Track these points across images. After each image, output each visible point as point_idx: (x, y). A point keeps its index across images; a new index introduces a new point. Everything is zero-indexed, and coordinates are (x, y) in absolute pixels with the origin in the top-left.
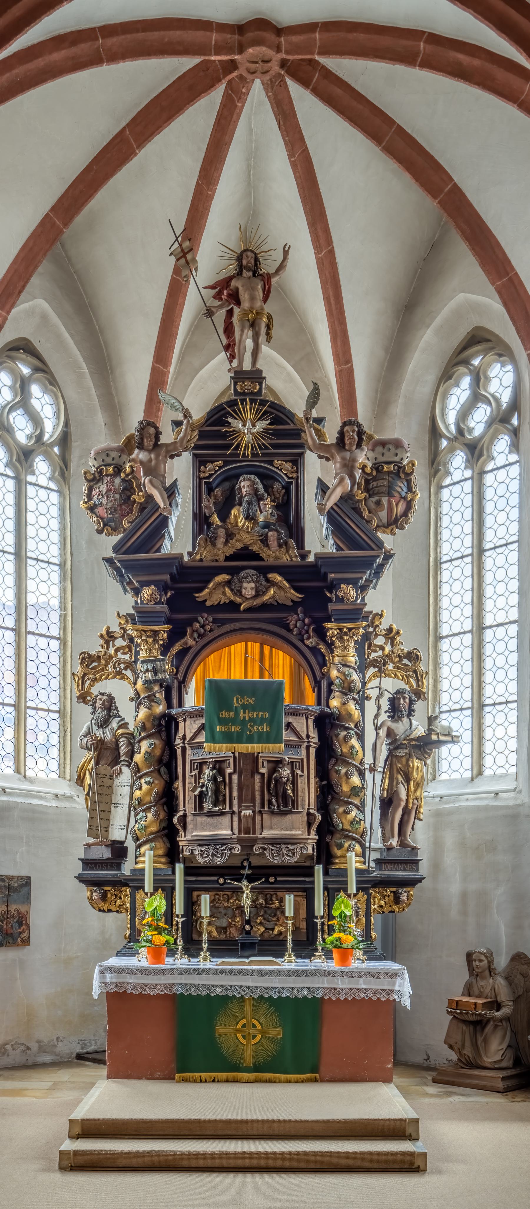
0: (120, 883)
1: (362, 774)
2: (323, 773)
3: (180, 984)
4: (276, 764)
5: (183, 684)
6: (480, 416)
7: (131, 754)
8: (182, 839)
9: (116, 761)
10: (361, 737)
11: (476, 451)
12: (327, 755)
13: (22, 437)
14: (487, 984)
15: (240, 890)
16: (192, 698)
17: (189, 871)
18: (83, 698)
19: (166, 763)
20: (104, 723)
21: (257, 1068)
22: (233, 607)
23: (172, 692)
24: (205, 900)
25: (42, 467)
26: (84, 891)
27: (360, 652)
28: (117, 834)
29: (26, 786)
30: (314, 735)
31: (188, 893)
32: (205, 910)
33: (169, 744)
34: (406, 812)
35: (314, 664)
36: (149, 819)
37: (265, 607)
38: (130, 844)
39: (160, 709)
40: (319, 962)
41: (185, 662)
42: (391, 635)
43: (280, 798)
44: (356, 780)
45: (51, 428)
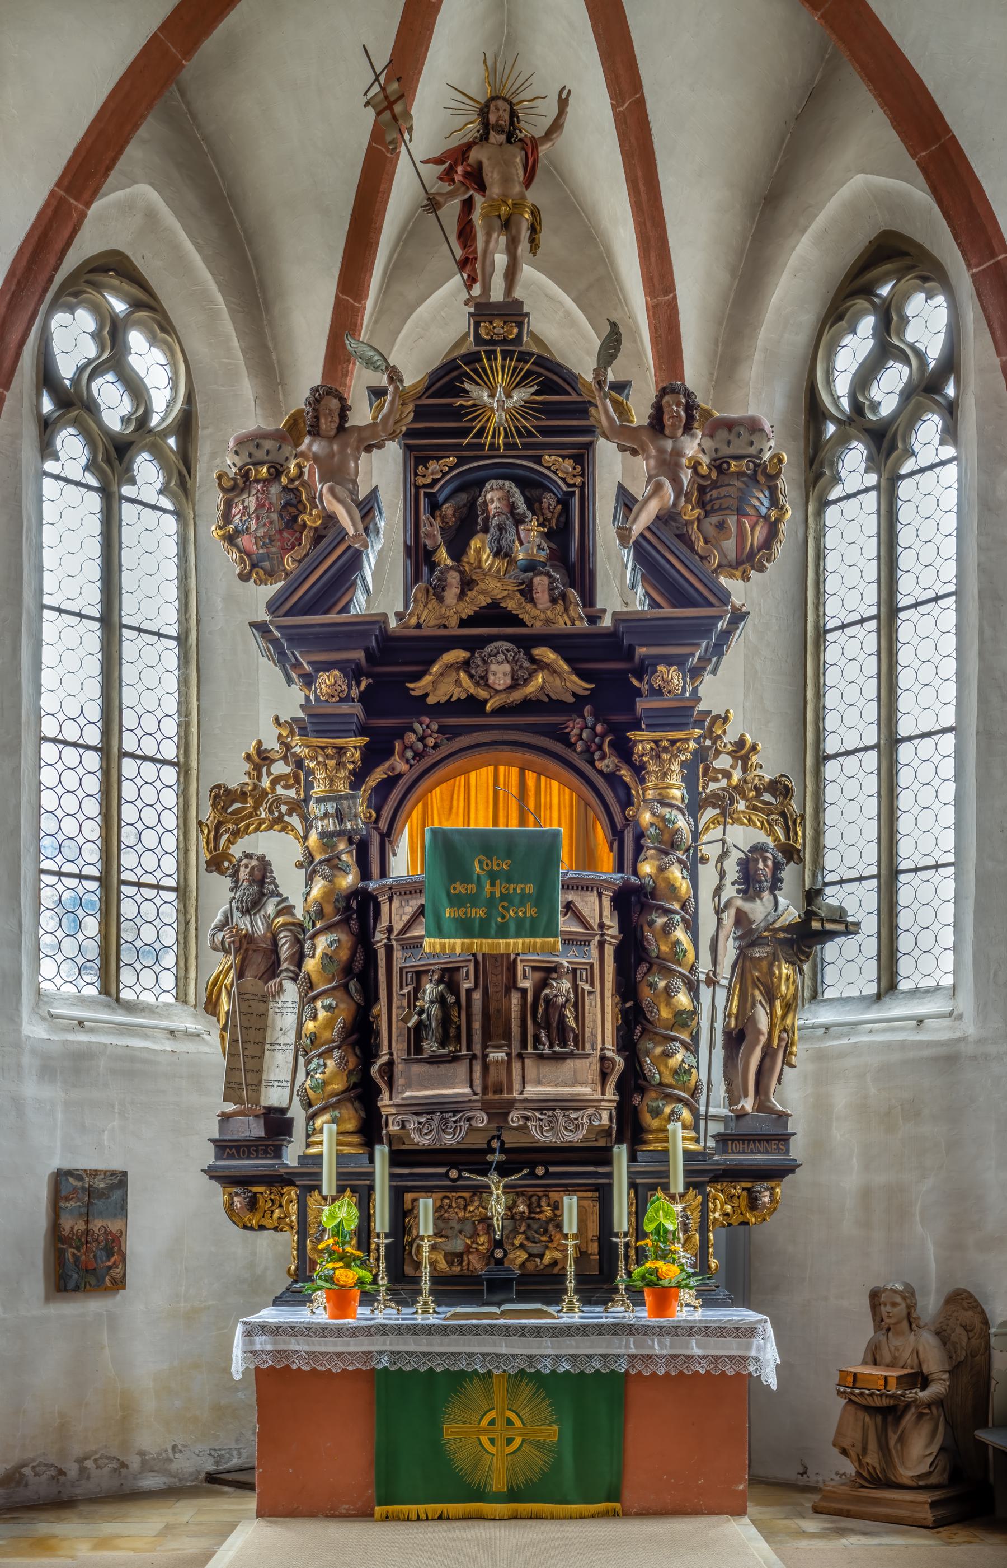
1: (693, 988)
2: (627, 989)
4: (548, 972)
5: (387, 837)
6: (887, 392)
7: (299, 959)
8: (386, 1103)
9: (273, 970)
10: (692, 927)
11: (887, 443)
12: (633, 956)
16: (403, 862)
17: (397, 1158)
19: (360, 974)
20: (252, 907)
21: (513, 1495)
22: (472, 705)
23: (369, 852)
25: (147, 473)
26: (217, 1194)
27: (690, 781)
28: (275, 1096)
30: (611, 922)
31: (397, 1195)
32: (425, 1224)
33: (363, 939)
34: (768, 1053)
36: (331, 1071)
37: (527, 706)
38: (298, 1113)
39: (348, 881)
40: (620, 1311)
41: (391, 800)
42: (742, 752)
44: (683, 999)
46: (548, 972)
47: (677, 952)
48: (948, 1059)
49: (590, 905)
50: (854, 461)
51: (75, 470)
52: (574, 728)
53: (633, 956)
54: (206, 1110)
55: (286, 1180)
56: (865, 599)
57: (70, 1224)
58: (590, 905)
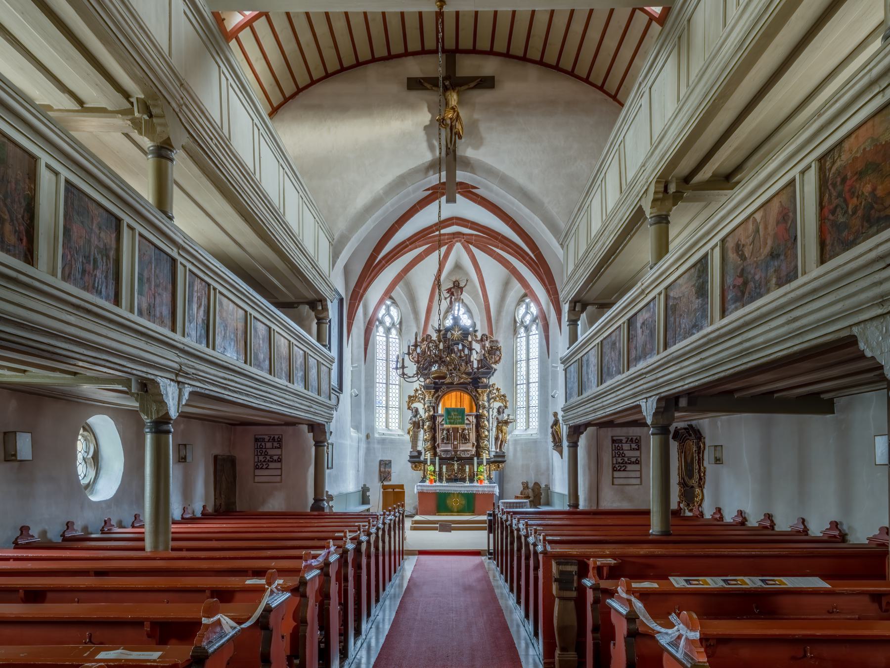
0: (421, 462)
1: (489, 431)
2: (477, 431)
3: (438, 490)
4: (464, 430)
5: (438, 405)
6: (528, 318)
7: (423, 425)
8: (438, 450)
9: (419, 427)
10: (488, 421)
11: (527, 329)
12: (478, 426)
13: (388, 324)
14: (526, 491)
15: (219, 623)
16: (440, 410)
17: (441, 459)
18: (409, 408)
19: (433, 429)
20: (415, 416)
21: (458, 512)
22: (452, 383)
23: (435, 408)
24: (444, 467)
25: (394, 332)
26: (410, 464)
27: (488, 396)
28: (420, 448)
29: (292, 340)
30: (475, 421)
31: (440, 465)
32: (444, 470)
33: (434, 423)
34: (502, 441)
35: (475, 399)
36: (429, 444)
37: (461, 384)
38: (423, 451)
39: (432, 413)
40: (475, 484)
41: (438, 399)
42: (498, 390)
43: (465, 439)
44: (486, 433)
45: (397, 320)
46: (464, 430)
47: (485, 426)
48: (535, 442)
49: (471, 418)
50: (522, 330)
51: (382, 334)
52: (469, 387)
53: (478, 426)
54: (409, 449)
55: (421, 462)
56: (524, 357)
57: (382, 469)
58: (471, 418)
